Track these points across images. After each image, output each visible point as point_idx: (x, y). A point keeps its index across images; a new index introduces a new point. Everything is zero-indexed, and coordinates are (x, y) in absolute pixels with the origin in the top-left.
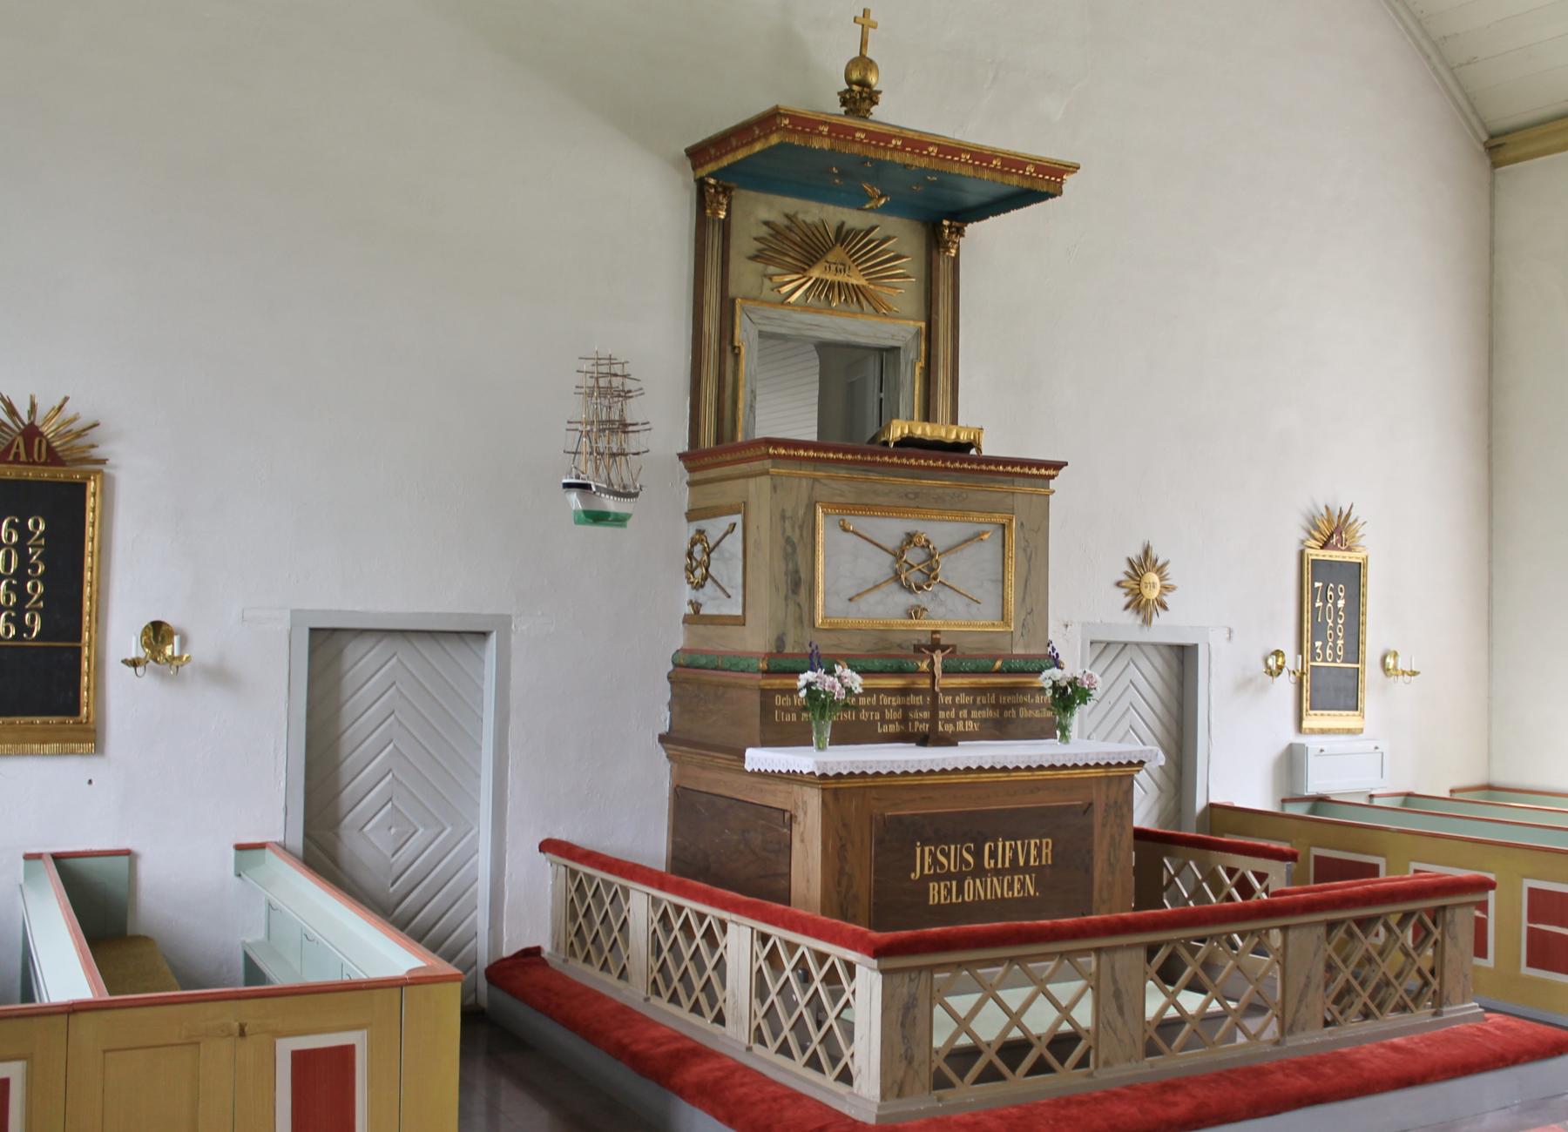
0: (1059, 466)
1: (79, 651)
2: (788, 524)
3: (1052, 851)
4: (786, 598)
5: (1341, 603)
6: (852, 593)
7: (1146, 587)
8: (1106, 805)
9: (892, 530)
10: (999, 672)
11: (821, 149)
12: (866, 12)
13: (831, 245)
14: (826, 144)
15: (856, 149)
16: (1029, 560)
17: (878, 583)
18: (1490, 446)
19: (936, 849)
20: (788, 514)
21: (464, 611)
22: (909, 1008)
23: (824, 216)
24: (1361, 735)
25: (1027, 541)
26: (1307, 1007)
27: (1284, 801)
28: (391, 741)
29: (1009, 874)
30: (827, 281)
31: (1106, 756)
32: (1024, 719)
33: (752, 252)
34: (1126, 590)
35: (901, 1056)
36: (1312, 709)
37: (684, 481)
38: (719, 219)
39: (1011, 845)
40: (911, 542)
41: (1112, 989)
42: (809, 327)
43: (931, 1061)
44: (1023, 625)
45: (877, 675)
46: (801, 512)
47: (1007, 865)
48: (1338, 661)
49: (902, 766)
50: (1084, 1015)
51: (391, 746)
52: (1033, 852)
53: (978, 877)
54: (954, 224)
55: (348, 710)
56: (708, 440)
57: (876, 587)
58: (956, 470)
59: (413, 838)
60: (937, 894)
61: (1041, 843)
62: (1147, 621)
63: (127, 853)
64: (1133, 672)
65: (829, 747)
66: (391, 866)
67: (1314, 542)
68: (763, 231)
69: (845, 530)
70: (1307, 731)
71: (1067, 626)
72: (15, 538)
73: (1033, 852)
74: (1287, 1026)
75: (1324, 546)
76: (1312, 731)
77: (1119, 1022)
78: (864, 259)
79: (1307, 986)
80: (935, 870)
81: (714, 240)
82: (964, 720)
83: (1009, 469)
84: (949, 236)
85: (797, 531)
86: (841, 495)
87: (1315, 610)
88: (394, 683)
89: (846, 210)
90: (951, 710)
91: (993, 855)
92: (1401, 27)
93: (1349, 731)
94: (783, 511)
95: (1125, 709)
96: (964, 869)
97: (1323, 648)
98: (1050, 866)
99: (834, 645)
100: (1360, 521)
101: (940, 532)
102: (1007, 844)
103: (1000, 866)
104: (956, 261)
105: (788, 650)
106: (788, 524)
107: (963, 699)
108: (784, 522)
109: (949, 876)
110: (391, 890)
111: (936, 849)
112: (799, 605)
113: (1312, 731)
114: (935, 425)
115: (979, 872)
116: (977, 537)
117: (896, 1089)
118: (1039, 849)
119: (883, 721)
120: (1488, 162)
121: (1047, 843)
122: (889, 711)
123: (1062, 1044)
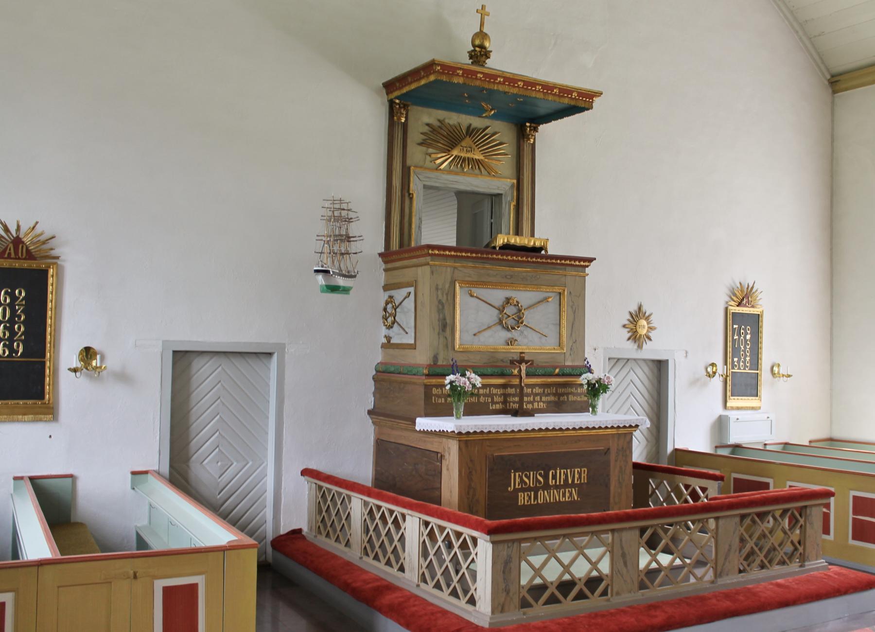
0: (591, 260)
1: (44, 363)
2: (440, 293)
3: (587, 475)
4: (439, 334)
5: (748, 337)
6: (476, 331)
7: (640, 328)
8: (617, 449)
9: (498, 296)
10: (558, 375)
11: (458, 83)
12: (483, 7)
13: (464, 137)
14: (461, 80)
15: (478, 83)
16: (574, 313)
17: (490, 326)
18: (831, 249)
19: (522, 474)
20: (440, 287)
21: (259, 341)
22: (507, 563)
23: (460, 121)
24: (759, 411)
25: (573, 302)
26: (729, 562)
27: (716, 447)
28: (218, 414)
29: (563, 488)
30: (462, 157)
31: (617, 422)
32: (572, 401)
33: (420, 141)
34: (628, 330)
35: (503, 589)
36: (732, 396)
37: (382, 269)
38: (401, 122)
39: (564, 472)
40: (508, 303)
42: (452, 183)
43: (520, 593)
44: (571, 349)
45: (489, 377)
46: (447, 286)
47: (562, 483)
48: (747, 369)
49: (504, 427)
50: (605, 567)
51: (218, 416)
52: (577, 476)
53: (546, 490)
54: (532, 125)
55: (194, 396)
56: (395, 245)
57: (489, 327)
58: (533, 262)
59: (231, 468)
60: (523, 499)
61: (581, 471)
62: (640, 347)
63: (71, 476)
65: (462, 417)
66: (218, 483)
67: (733, 302)
68: (426, 129)
69: (472, 296)
70: (730, 408)
71: (595, 349)
72: (8, 301)
73: (577, 476)
74: (718, 573)
75: (739, 305)
76: (732, 408)
77: (624, 570)
78: (482, 144)
79: (729, 550)
80: (522, 486)
81: (399, 134)
82: (538, 402)
83: (563, 262)
84: (529, 132)
85: (445, 297)
86: (469, 277)
87: (734, 341)
88: (220, 382)
89: (472, 117)
90: (531, 397)
91: (554, 477)
92: (782, 15)
93: (753, 408)
94: (437, 285)
95: (628, 396)
96: (538, 485)
97: (738, 362)
98: (586, 483)
99: (465, 360)
100: (759, 291)
101: (525, 297)
102: (562, 471)
103: (558, 483)
104: (533, 146)
105: (440, 363)
106: (440, 293)
107: (537, 390)
108: (438, 291)
109: (529, 489)
110: (218, 497)
111: (522, 474)
112: (446, 338)
113: (732, 408)
114: (522, 237)
115: (546, 487)
116: (545, 300)
117: (500, 608)
118: (580, 474)
119: (493, 402)
120: (830, 90)
121: (584, 471)
122: (496, 397)
123: (593, 583)
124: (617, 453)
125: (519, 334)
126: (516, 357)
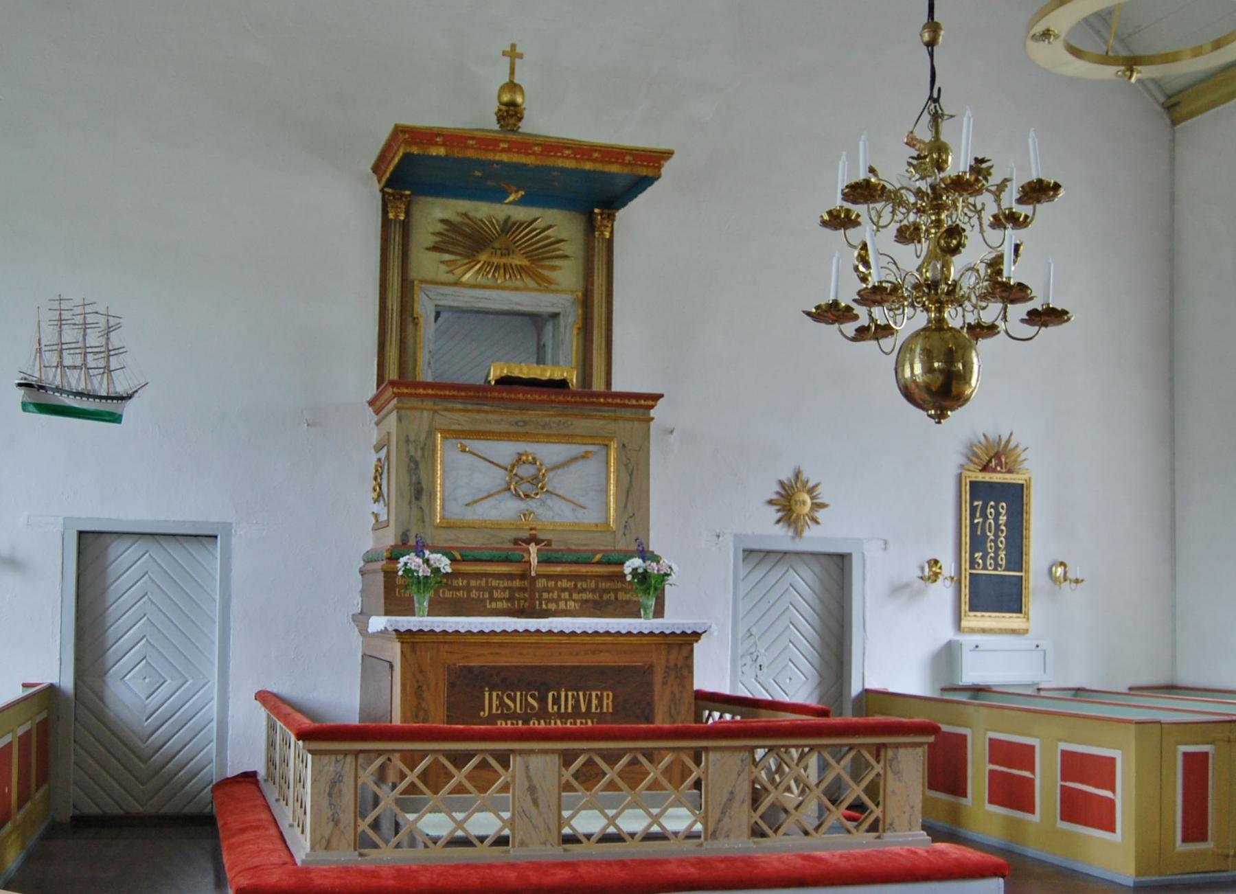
3: (613, 701)
4: (410, 503)
5: (1003, 519)
6: (469, 499)
7: (796, 504)
8: (667, 667)
9: (505, 451)
10: (599, 563)
11: (437, 157)
12: (513, 46)
13: (497, 235)
14: (442, 151)
16: (631, 474)
17: (492, 492)
18: (1171, 379)
19: (503, 694)
20: (412, 438)
21: (195, 519)
22: (335, 782)
24: (1027, 635)
25: (629, 459)
26: (731, 818)
28: (145, 615)
29: (571, 718)
30: (493, 263)
31: (660, 626)
33: (430, 244)
34: (778, 507)
35: (328, 818)
36: (971, 610)
37: (373, 422)
38: (400, 220)
39: (573, 695)
41: (526, 784)
43: (356, 826)
44: (625, 526)
45: (487, 563)
46: (423, 437)
47: (570, 710)
48: (999, 569)
49: (466, 626)
51: (145, 618)
52: (594, 702)
53: (542, 718)
55: (112, 593)
57: (490, 496)
58: (559, 402)
59: (162, 688)
61: (602, 694)
62: (798, 533)
64: (793, 576)
66: (145, 706)
67: (972, 465)
68: (440, 227)
69: (464, 451)
70: (966, 630)
71: (718, 536)
73: (594, 702)
74: (710, 833)
75: (985, 468)
76: (972, 631)
78: (526, 244)
79: (730, 800)
80: (502, 711)
82: (566, 601)
84: (601, 222)
85: (419, 453)
86: (459, 424)
87: (973, 527)
88: (146, 573)
90: (553, 593)
91: (556, 701)
93: (1013, 632)
94: (407, 436)
95: (785, 607)
96: (529, 711)
97: (984, 558)
98: (611, 713)
99: (451, 540)
100: (1022, 447)
101: (549, 452)
102: (570, 694)
103: (563, 710)
104: (610, 243)
110: (146, 723)
111: (503, 694)
112: (421, 508)
113: (972, 631)
114: (545, 367)
115: (543, 714)
116: (584, 456)
117: (324, 843)
118: (600, 699)
119: (492, 599)
120: (1168, 122)
121: (608, 695)
122: (497, 591)
124: (665, 672)
125: (539, 504)
126: (525, 534)
